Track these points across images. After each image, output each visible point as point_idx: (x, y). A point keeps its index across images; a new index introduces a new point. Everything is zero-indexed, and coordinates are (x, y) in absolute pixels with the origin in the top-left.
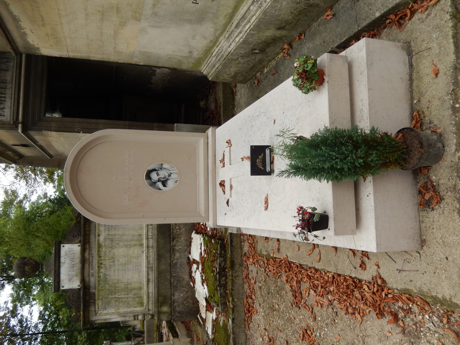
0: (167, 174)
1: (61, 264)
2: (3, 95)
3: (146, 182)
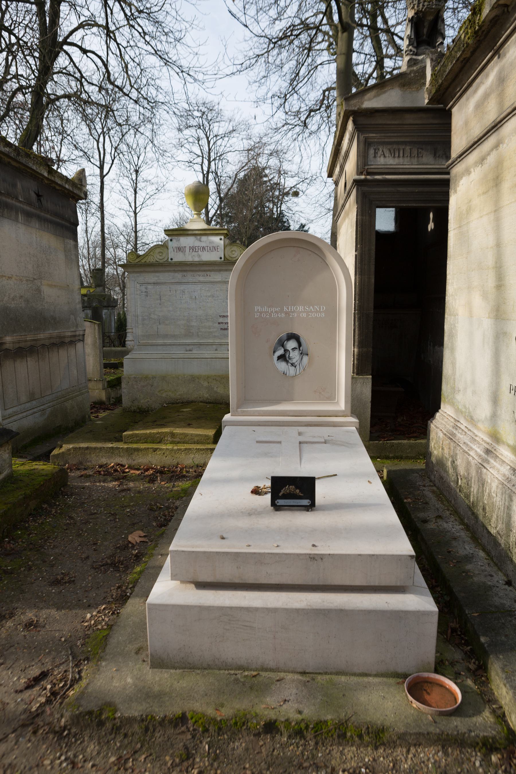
0: (294, 361)
2: (401, 155)
3: (284, 334)
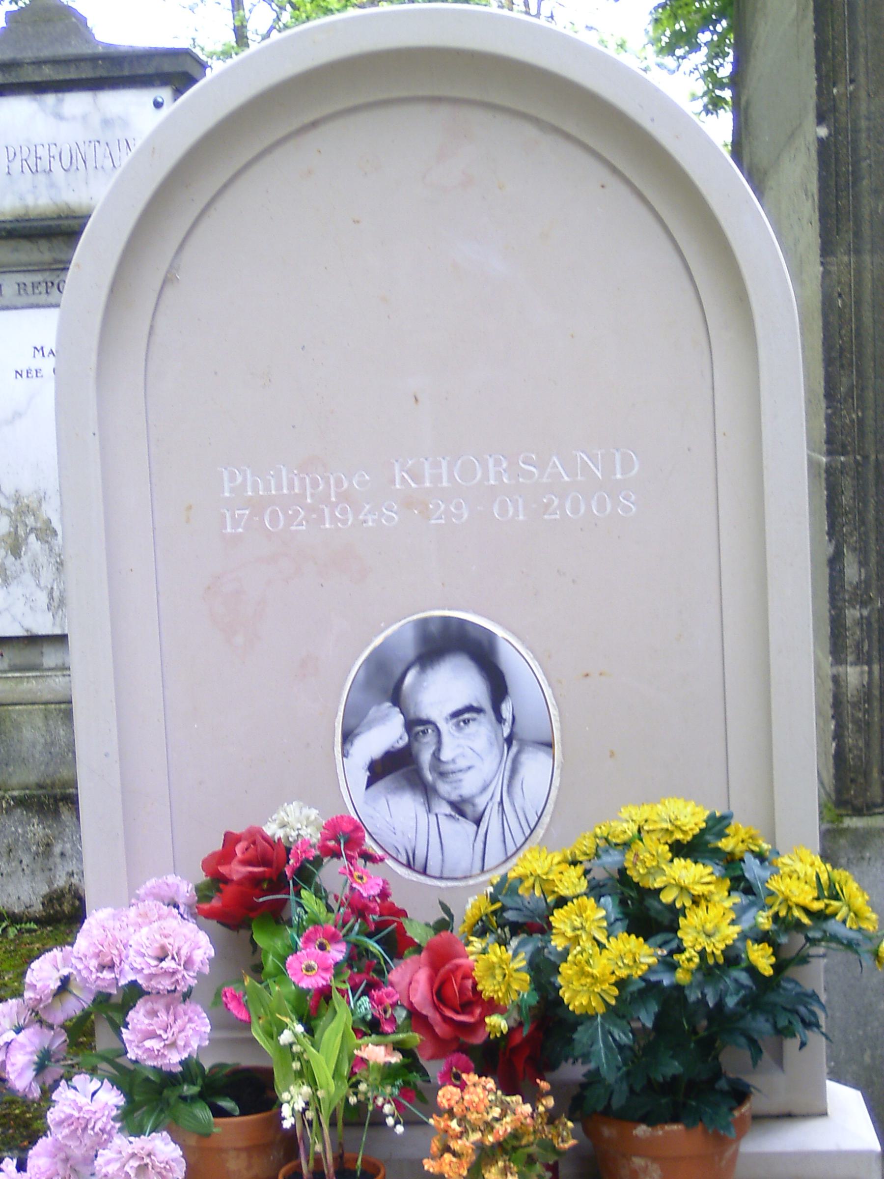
0: (468, 785)
1: (50, 99)
3: (396, 629)
